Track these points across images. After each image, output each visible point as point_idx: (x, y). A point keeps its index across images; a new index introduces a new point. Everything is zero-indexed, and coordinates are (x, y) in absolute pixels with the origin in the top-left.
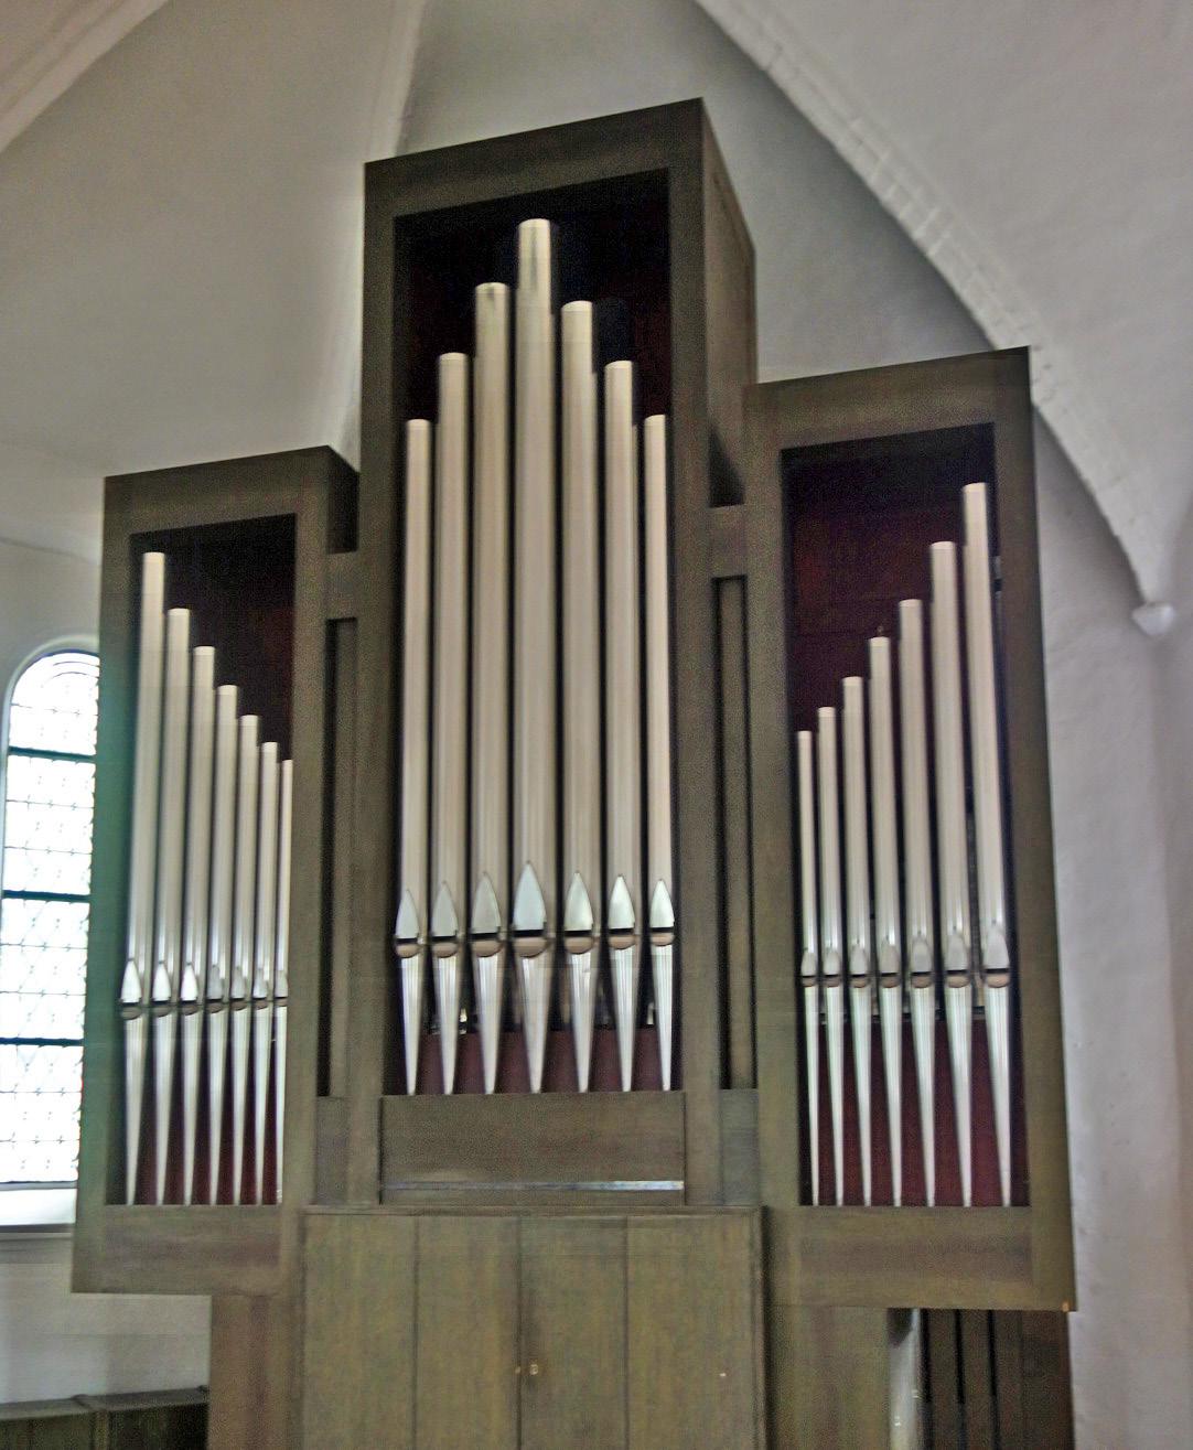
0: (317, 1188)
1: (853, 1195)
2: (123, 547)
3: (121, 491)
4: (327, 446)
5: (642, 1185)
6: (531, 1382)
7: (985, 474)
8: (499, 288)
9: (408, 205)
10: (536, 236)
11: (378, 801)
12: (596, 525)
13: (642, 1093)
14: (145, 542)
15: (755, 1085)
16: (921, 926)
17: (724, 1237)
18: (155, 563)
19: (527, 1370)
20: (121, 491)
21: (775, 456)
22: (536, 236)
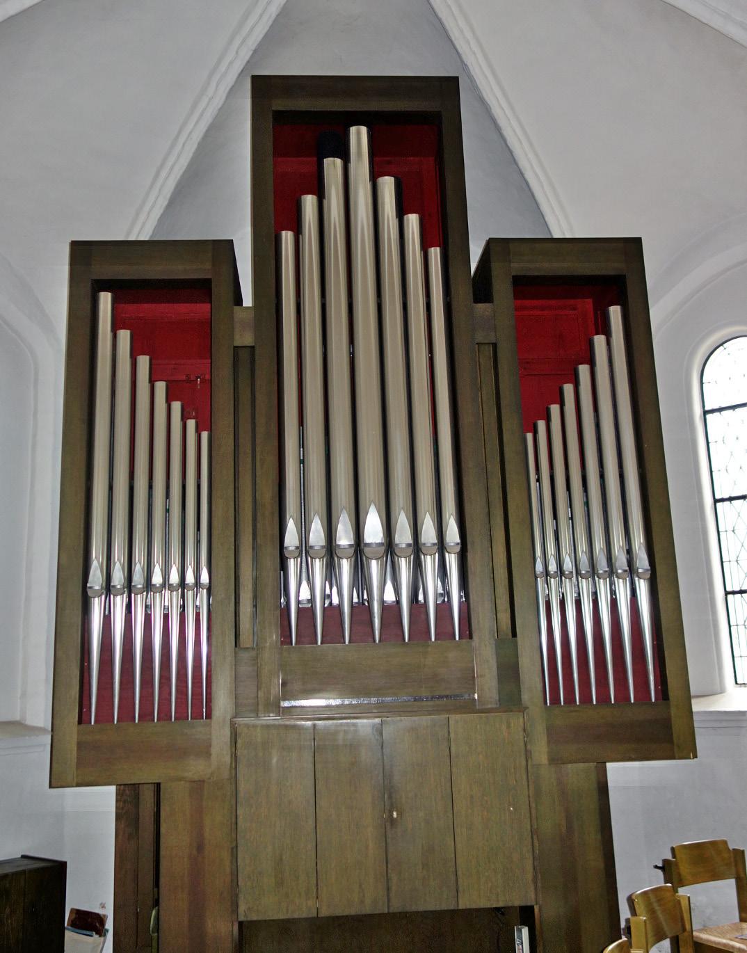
0: (237, 705)
1: (586, 697)
2: (87, 289)
3: (82, 252)
4: (490, 239)
5: (652, 678)
6: (392, 821)
7: (622, 301)
8: (338, 161)
9: (280, 104)
10: (359, 137)
11: (272, 460)
12: (354, 309)
13: (381, 643)
14: (101, 285)
15: (514, 634)
16: (599, 545)
17: (509, 727)
18: (106, 299)
19: (392, 815)
20: (82, 252)
21: (509, 281)
22: (359, 137)
